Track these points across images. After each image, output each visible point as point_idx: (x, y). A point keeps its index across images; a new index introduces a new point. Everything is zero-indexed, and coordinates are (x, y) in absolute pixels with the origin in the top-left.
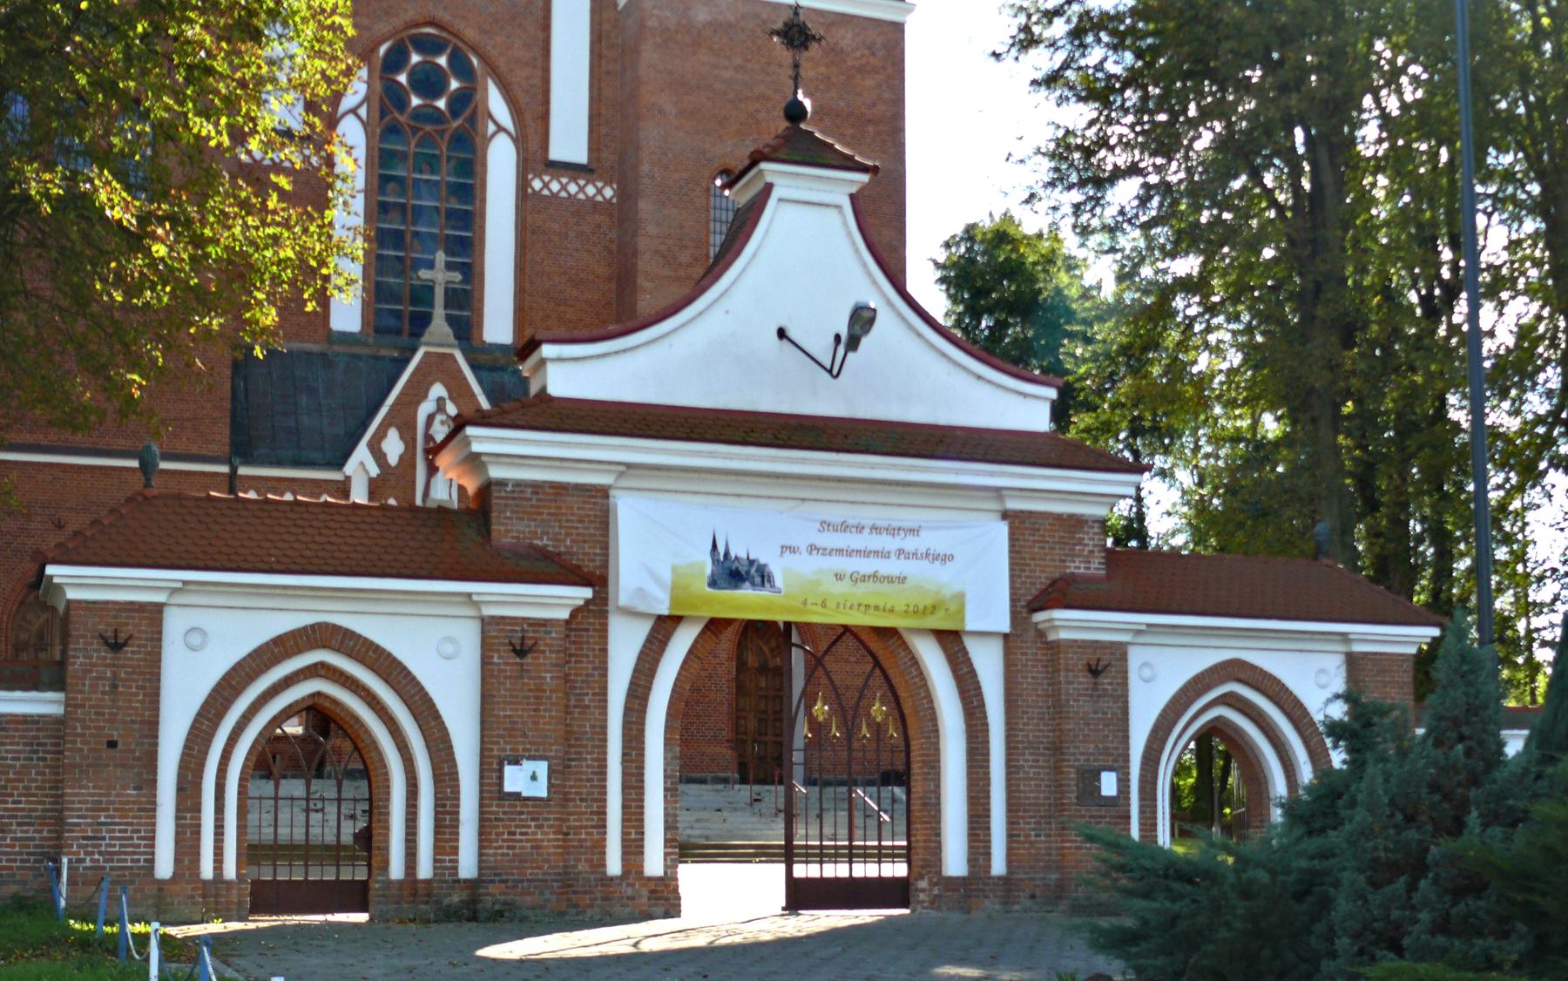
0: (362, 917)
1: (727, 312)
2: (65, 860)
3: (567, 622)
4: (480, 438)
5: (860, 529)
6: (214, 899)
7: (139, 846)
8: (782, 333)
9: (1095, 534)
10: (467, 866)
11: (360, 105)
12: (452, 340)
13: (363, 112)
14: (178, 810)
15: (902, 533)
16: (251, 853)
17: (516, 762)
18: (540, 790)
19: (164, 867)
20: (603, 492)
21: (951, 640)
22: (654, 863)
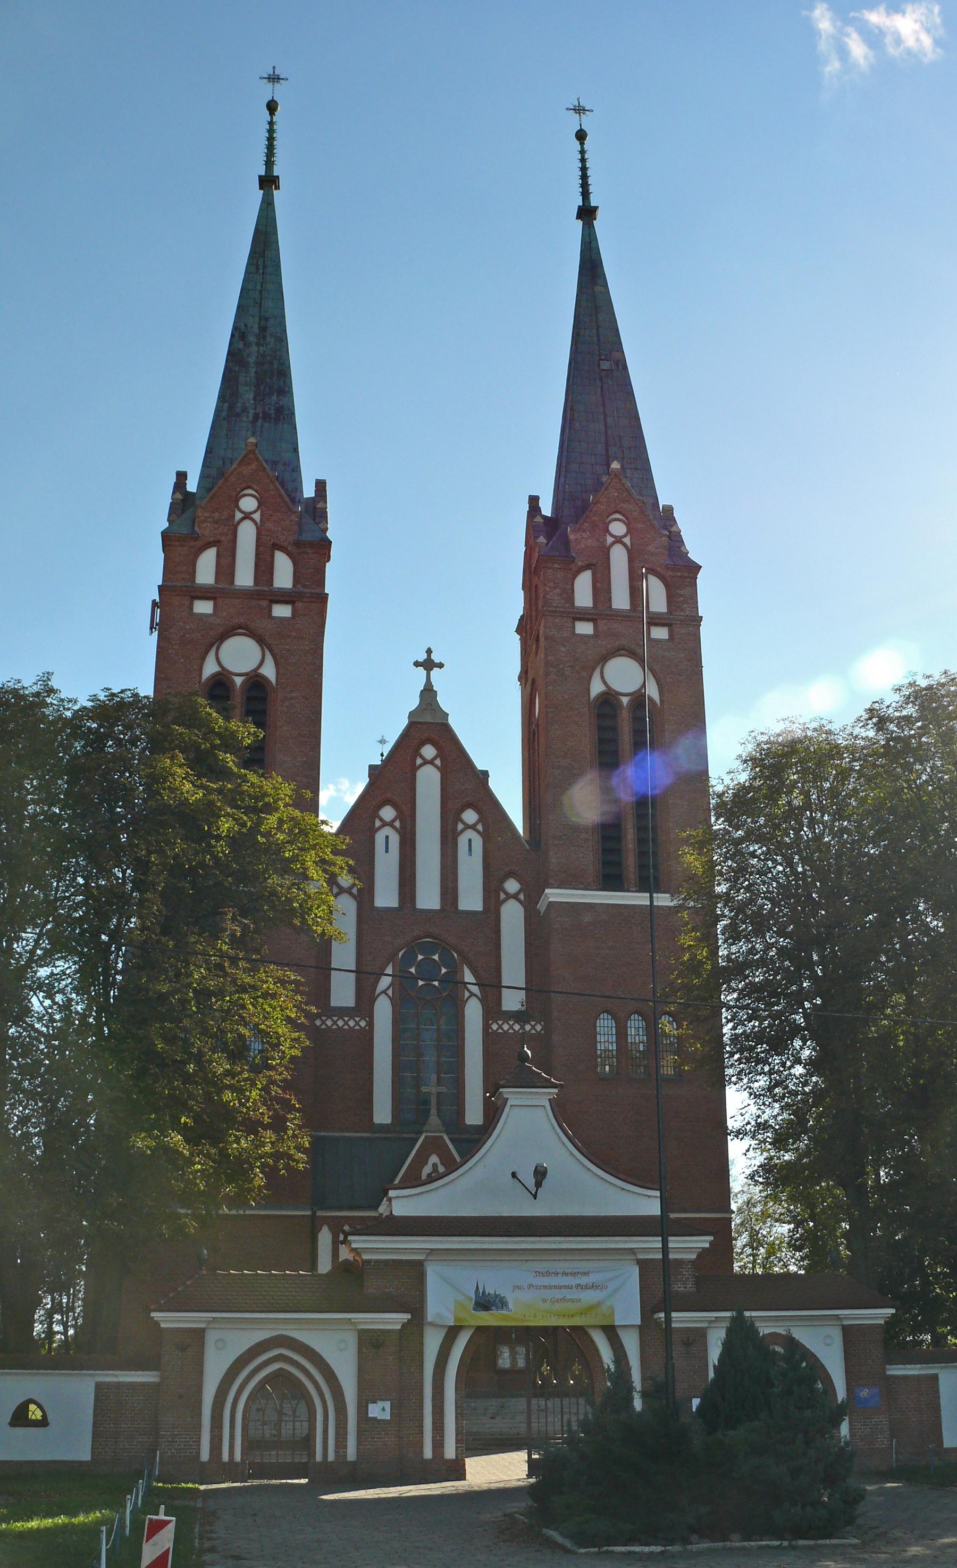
0: (304, 1481)
1: (485, 1166)
2: (158, 1452)
3: (400, 1330)
4: (355, 1241)
5: (557, 1274)
6: (230, 1471)
7: (192, 1445)
8: (514, 1175)
9: (689, 1268)
10: (351, 1453)
11: (388, 988)
12: (442, 1128)
13: (390, 992)
14: (212, 1428)
15: (579, 1274)
16: (250, 1445)
17: (375, 1402)
18: (387, 1416)
19: (205, 1456)
20: (420, 1264)
21: (611, 1331)
22: (450, 1452)
